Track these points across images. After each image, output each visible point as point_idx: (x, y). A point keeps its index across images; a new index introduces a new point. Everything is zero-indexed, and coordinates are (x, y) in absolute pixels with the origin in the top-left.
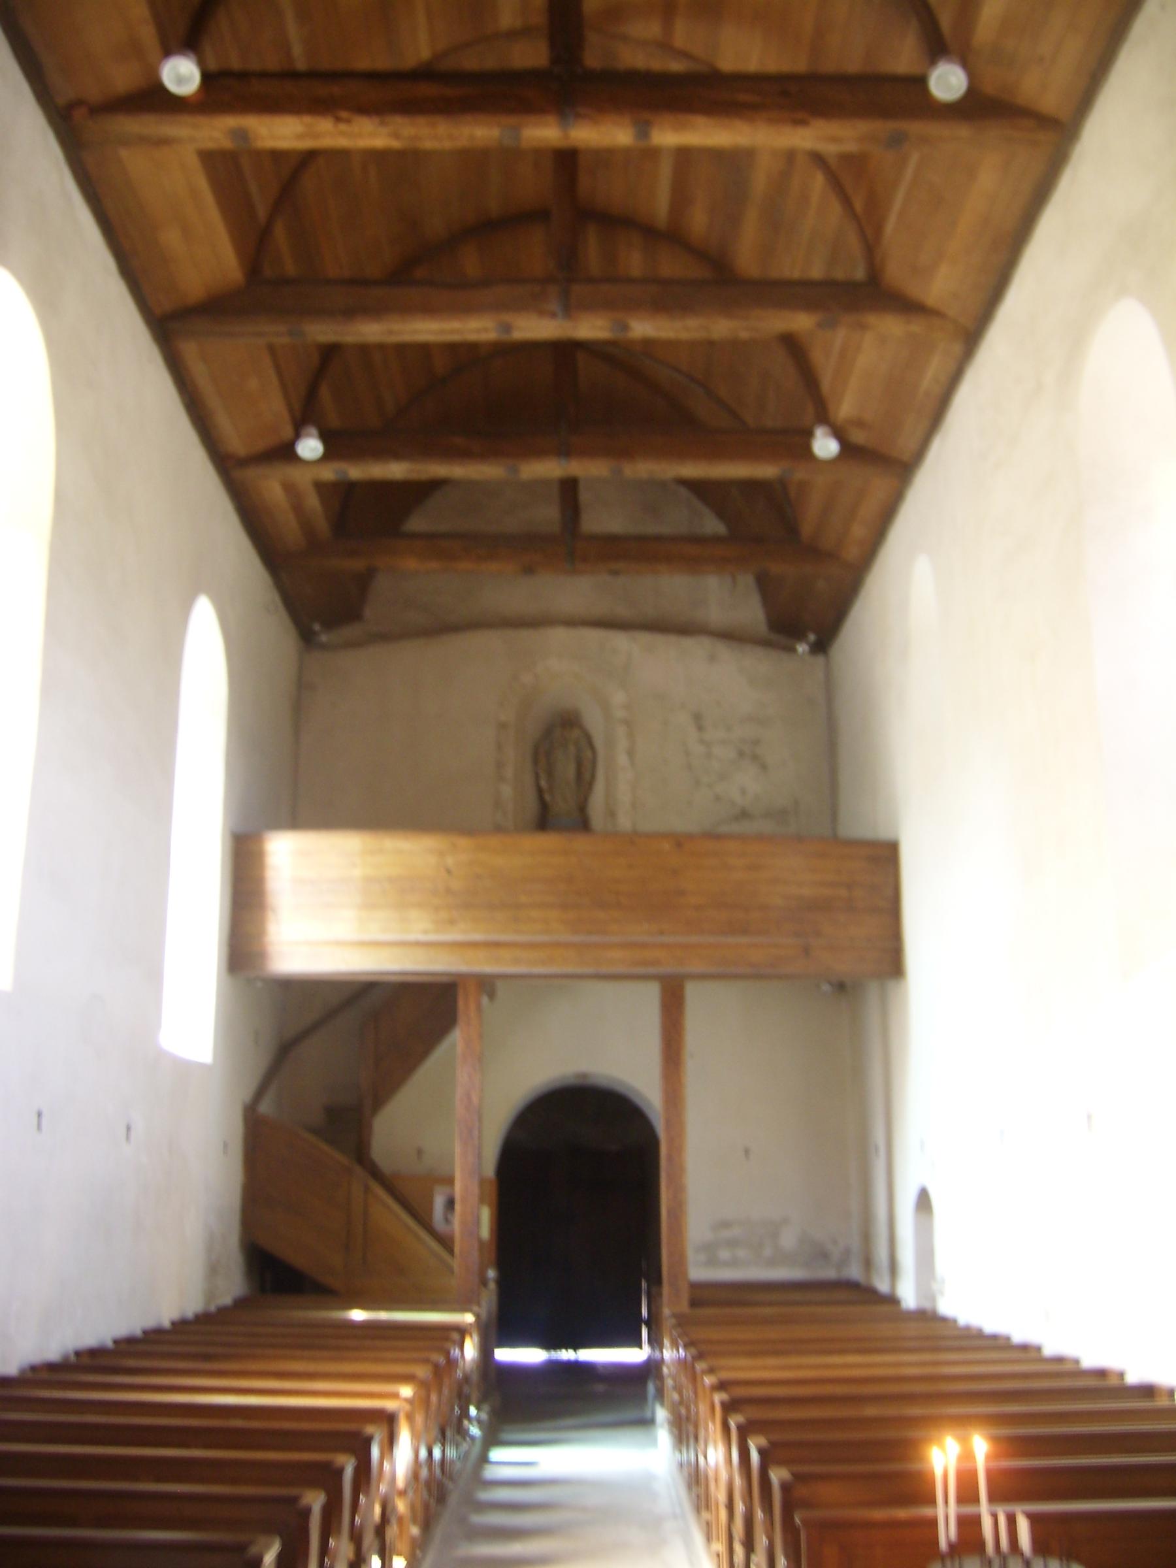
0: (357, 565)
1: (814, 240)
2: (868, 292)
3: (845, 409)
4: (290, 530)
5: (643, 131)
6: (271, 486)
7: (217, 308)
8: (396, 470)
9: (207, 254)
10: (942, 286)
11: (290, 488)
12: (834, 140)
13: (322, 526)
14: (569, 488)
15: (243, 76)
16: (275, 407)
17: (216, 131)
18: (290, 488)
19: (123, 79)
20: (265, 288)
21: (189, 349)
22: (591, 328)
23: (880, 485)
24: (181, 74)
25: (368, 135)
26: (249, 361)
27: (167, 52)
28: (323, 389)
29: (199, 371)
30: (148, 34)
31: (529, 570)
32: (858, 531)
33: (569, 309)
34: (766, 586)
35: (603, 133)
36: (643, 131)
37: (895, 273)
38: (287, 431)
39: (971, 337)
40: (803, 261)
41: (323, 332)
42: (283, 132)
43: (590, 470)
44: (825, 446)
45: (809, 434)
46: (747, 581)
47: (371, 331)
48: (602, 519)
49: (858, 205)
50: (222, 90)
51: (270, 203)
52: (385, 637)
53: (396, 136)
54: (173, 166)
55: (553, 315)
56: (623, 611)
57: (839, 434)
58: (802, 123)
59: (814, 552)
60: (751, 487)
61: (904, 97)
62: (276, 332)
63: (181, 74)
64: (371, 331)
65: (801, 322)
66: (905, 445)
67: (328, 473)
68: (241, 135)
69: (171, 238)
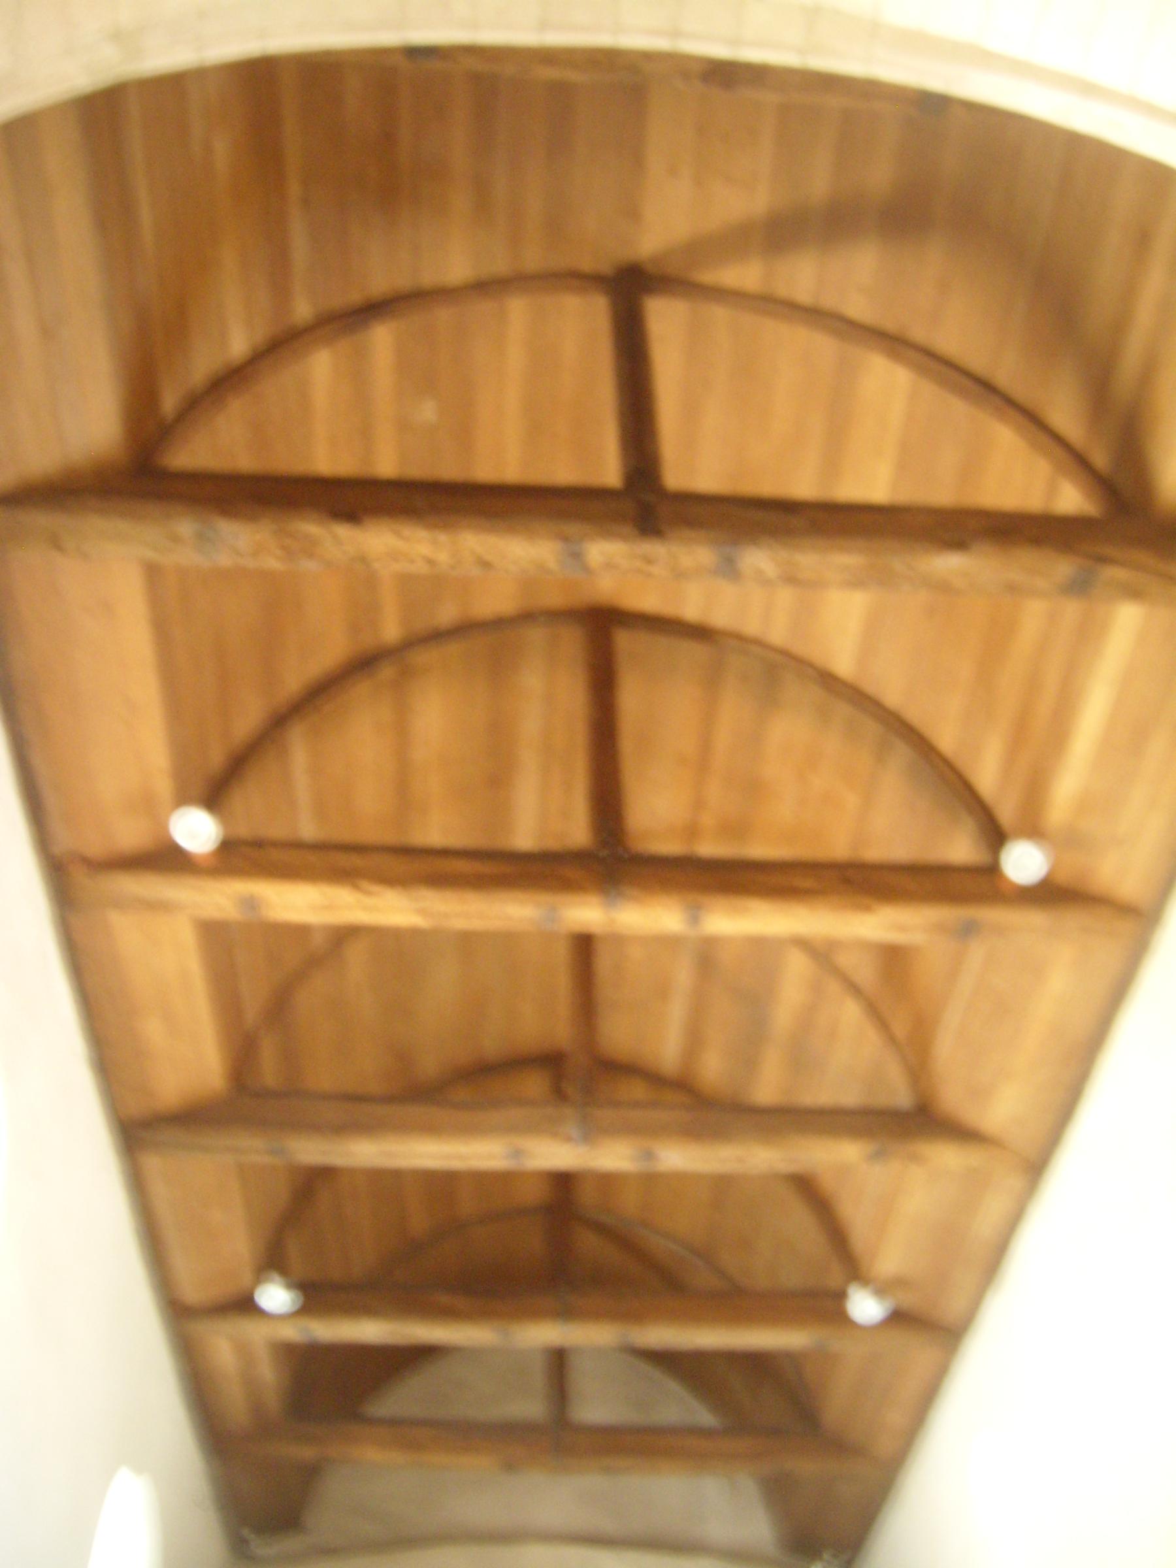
0: (307, 1453)
1: (852, 1060)
2: (917, 1120)
3: (890, 1260)
4: (235, 1405)
5: (694, 920)
6: (222, 1343)
7: (194, 1118)
8: (370, 1331)
9: (189, 1055)
10: (1005, 1108)
11: (243, 1350)
12: (902, 928)
13: (273, 1400)
14: (559, 1359)
15: (259, 844)
16: (239, 1245)
17: (221, 898)
18: (243, 1350)
19: (130, 835)
20: (252, 1096)
21: (153, 1163)
22: (613, 1156)
23: (919, 1354)
24: (195, 830)
25: (393, 909)
26: (220, 1183)
27: (183, 799)
28: (300, 1225)
29: (160, 1191)
30: (164, 786)
31: (510, 1466)
32: (895, 1418)
33: (591, 1133)
34: (779, 1492)
35: (645, 919)
36: (694, 920)
37: (953, 1097)
38: (247, 1277)
39: (1035, 1167)
40: (835, 1087)
41: (311, 1151)
42: (299, 903)
43: (589, 1336)
44: (865, 1307)
45: (840, 1296)
46: (748, 1487)
47: (366, 1152)
48: (595, 1406)
49: (900, 1029)
50: (237, 856)
51: (269, 990)
52: (329, 1552)
53: (421, 912)
54: (165, 940)
55: (568, 1139)
56: (607, 1525)
57: (881, 1291)
58: (867, 909)
59: (840, 1446)
60: (757, 1365)
61: (981, 883)
62: (255, 1147)
63: (195, 830)
64: (366, 1152)
65: (836, 1157)
66: (952, 1307)
67: (291, 1333)
68: (251, 903)
69: (153, 1030)
